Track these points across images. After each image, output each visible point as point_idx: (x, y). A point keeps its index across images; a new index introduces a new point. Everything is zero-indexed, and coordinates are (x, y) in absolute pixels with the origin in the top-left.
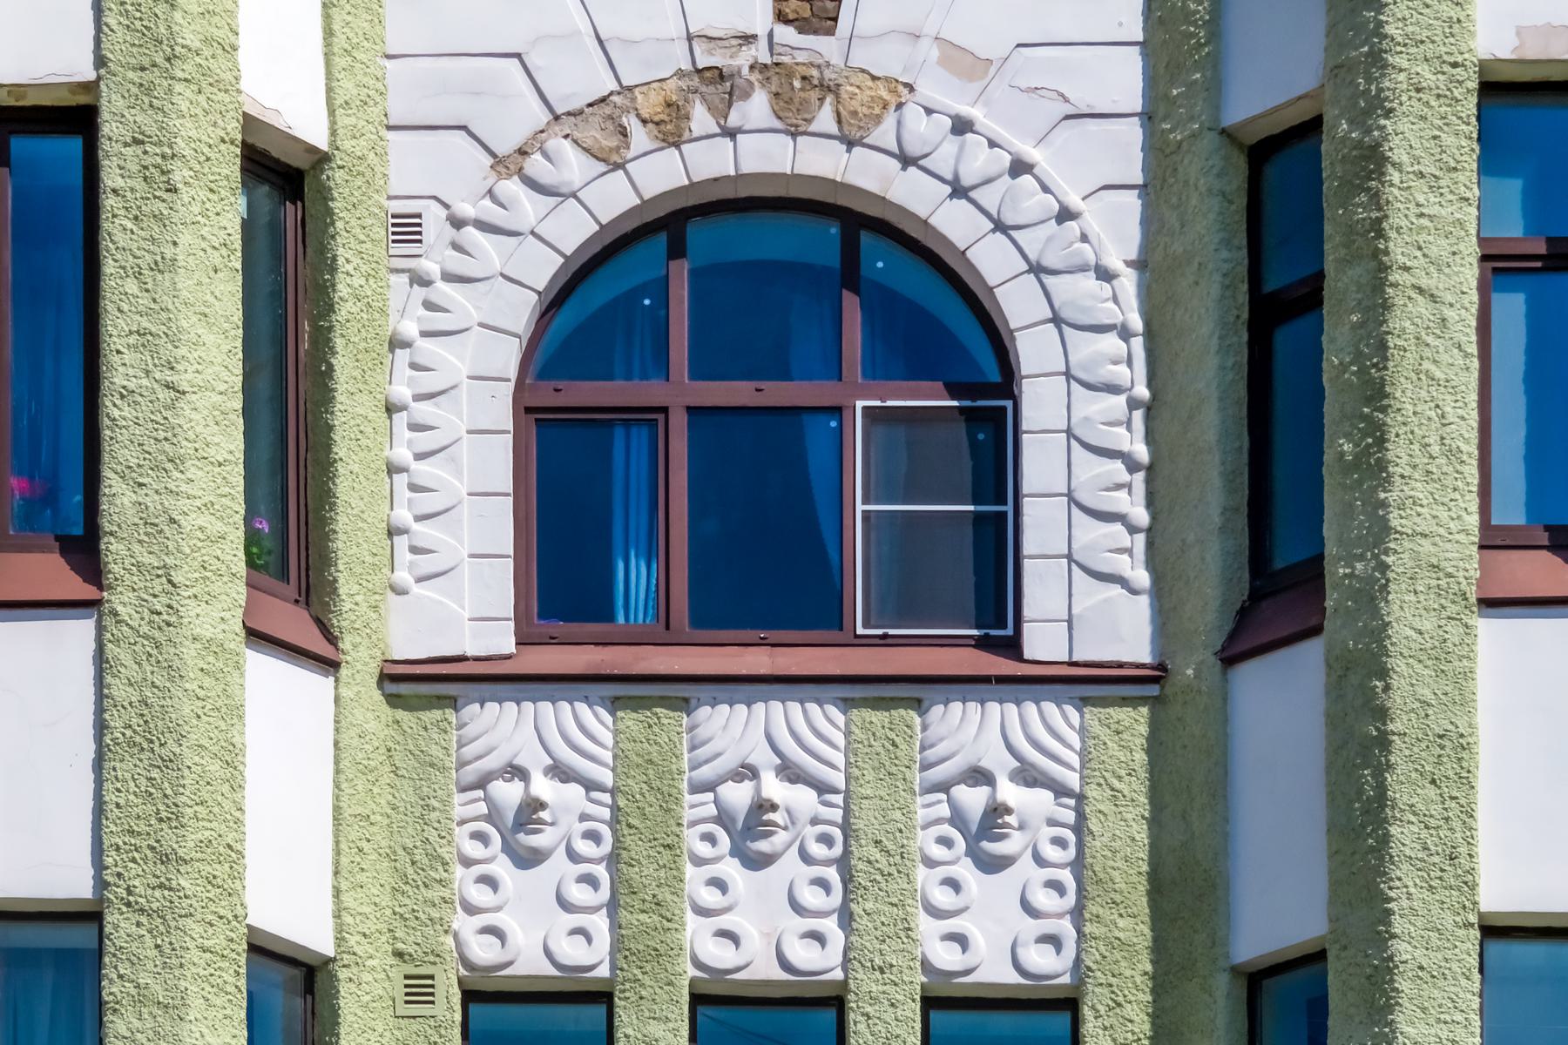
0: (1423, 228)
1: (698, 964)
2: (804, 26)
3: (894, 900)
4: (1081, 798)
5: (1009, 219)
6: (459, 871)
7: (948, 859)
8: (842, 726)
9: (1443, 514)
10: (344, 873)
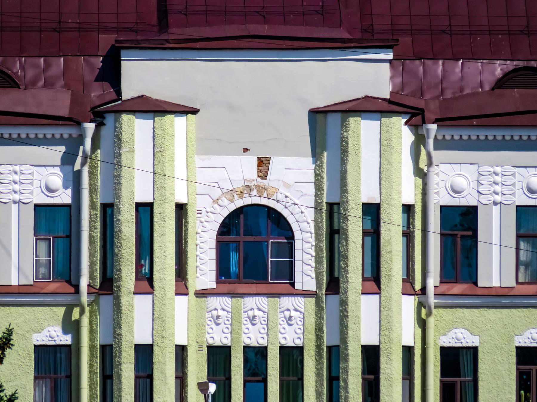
0: (353, 231)
1: (244, 343)
2: (262, 178)
6: (207, 326)
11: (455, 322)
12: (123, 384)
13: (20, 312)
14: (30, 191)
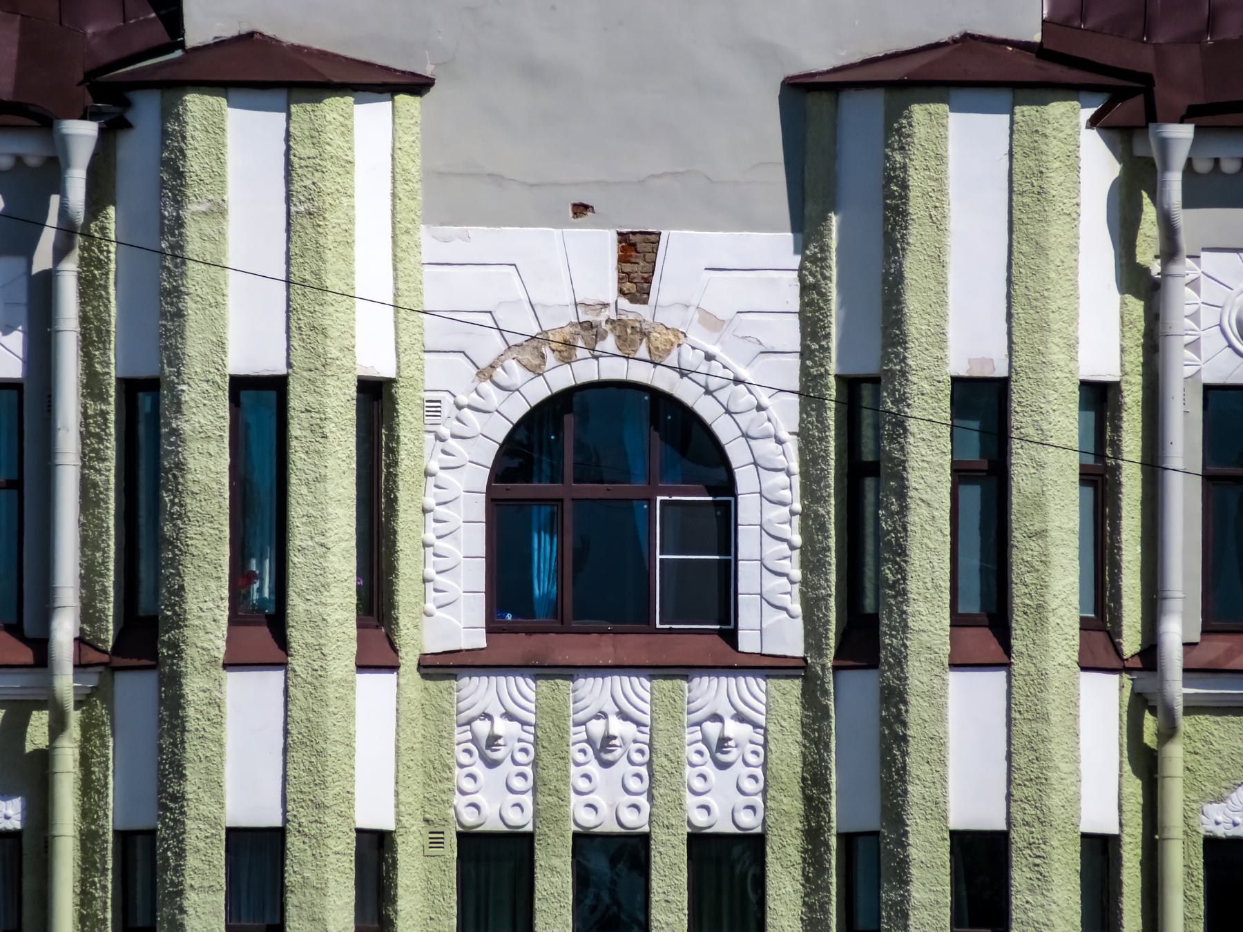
1: (576, 824)
3: (674, 788)
4: (766, 730)
5: (732, 409)
6: (457, 770)
7: (701, 763)
8: (649, 689)
9: (932, 619)
10: (401, 783)
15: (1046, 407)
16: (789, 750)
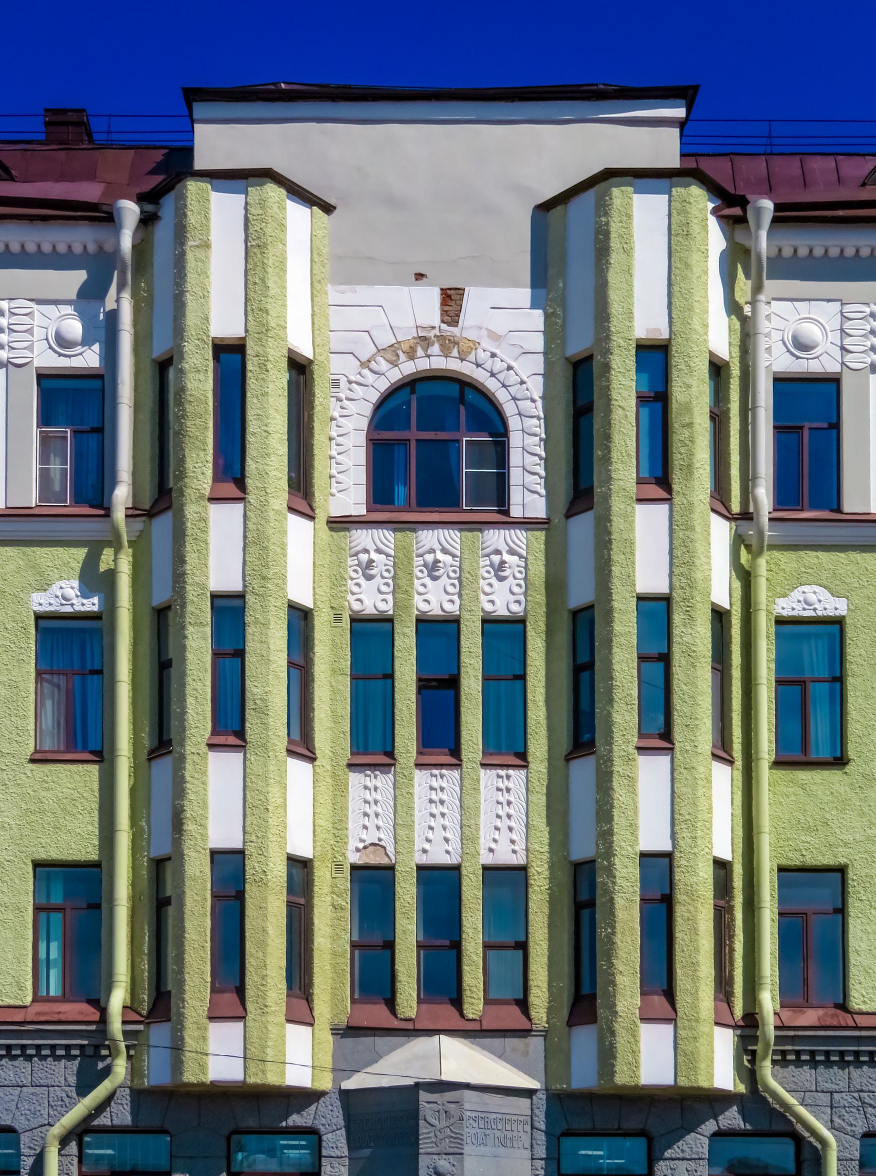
0: (620, 388)
1: (418, 610)
4: (526, 559)
6: (349, 581)
9: (626, 474)
11: (802, 572)
12: (189, 661)
13: (9, 554)
14: (26, 344)
15: (692, 354)
16: (538, 569)
